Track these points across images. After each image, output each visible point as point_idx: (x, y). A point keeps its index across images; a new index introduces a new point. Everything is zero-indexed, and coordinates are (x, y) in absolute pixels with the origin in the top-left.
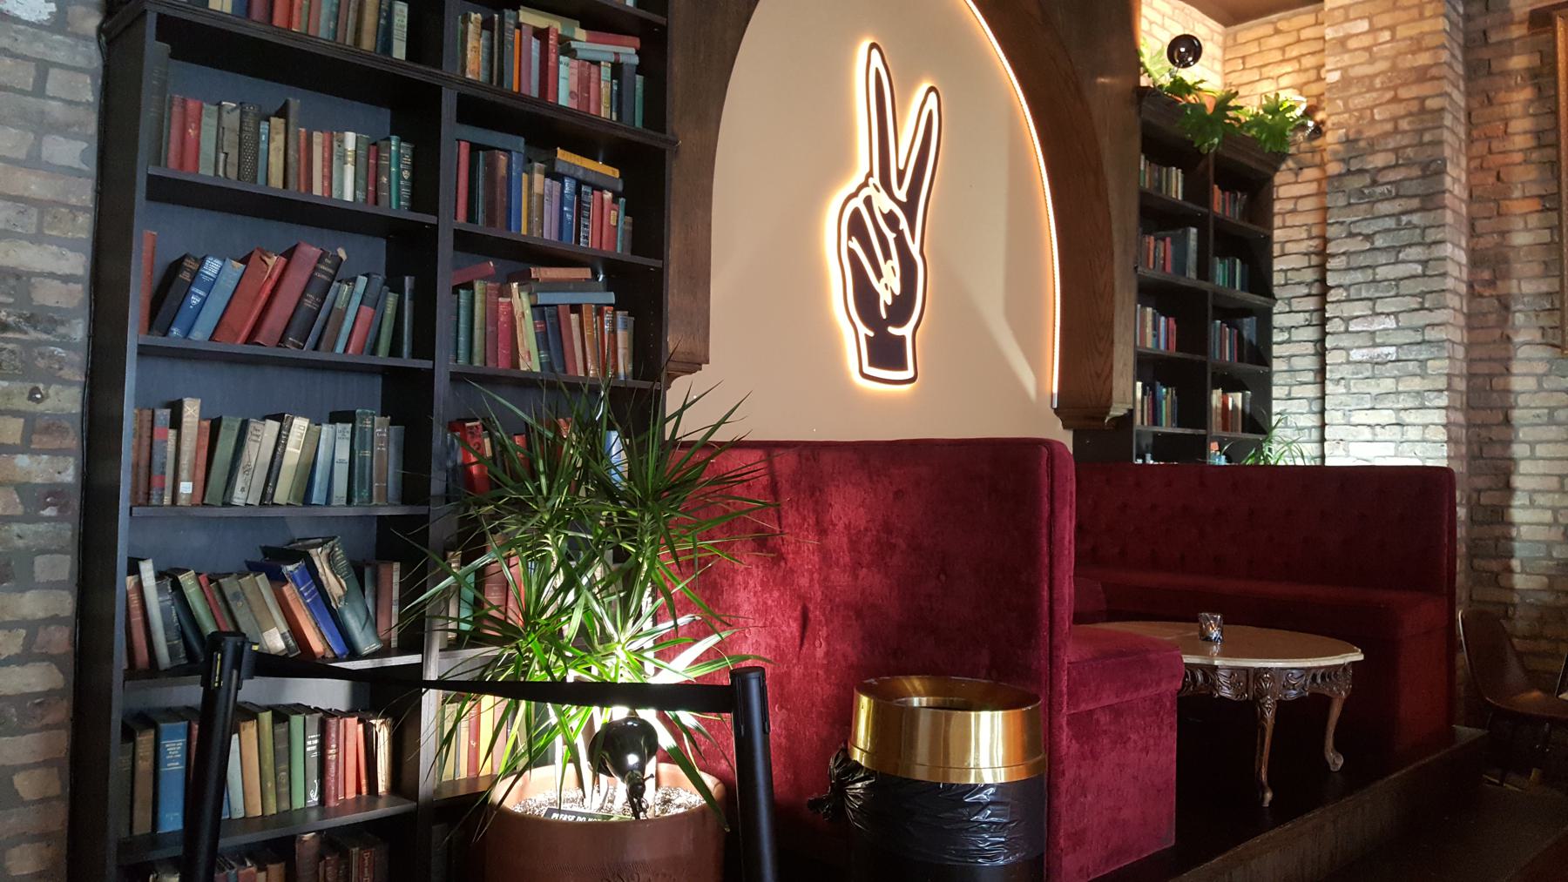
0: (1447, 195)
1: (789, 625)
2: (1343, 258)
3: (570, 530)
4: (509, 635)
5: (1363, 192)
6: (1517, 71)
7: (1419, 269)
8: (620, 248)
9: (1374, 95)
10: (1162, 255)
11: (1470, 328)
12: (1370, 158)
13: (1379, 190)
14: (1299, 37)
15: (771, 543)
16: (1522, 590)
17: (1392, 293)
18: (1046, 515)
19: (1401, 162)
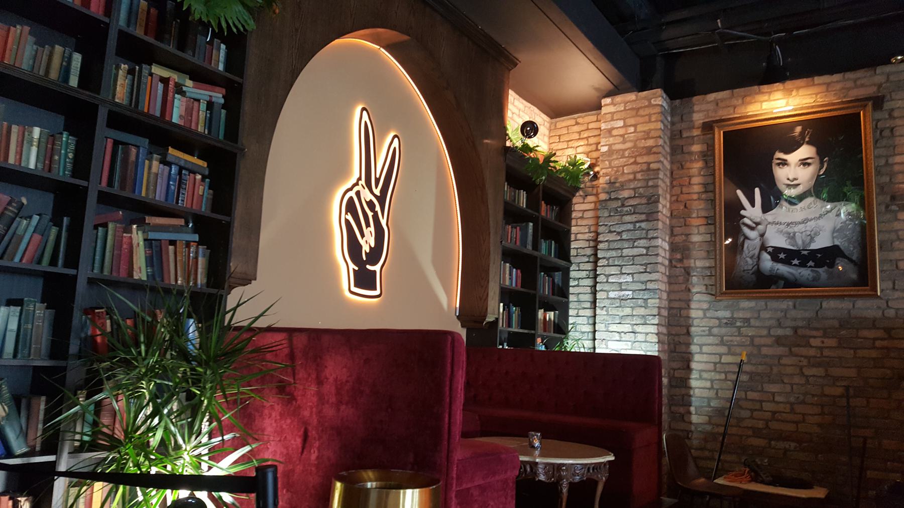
0: (660, 214)
1: (295, 441)
2: (606, 243)
3: (159, 379)
4: (114, 444)
5: (617, 210)
6: (696, 152)
7: (645, 251)
8: (204, 208)
9: (625, 160)
10: (515, 236)
11: (670, 283)
12: (621, 192)
13: (625, 209)
14: (588, 127)
15: (287, 389)
16: (697, 424)
17: (631, 263)
18: (449, 373)
19: (637, 195)
